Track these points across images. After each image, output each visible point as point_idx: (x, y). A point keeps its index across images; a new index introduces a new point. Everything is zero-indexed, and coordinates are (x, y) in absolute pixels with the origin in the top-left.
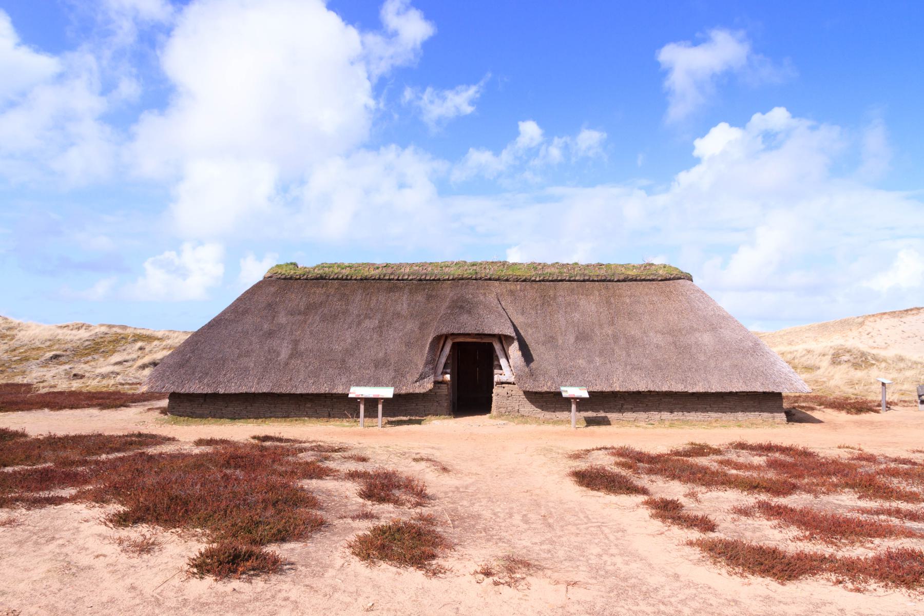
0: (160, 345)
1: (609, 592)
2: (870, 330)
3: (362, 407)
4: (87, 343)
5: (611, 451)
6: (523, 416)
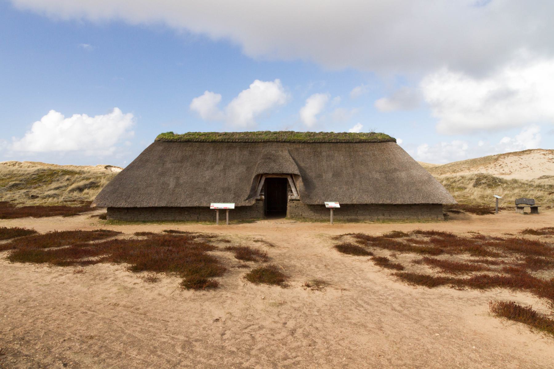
0: (80, 177)
1: (359, 292)
2: (501, 163)
3: (217, 214)
4: (34, 176)
5: (353, 235)
6: (304, 218)
